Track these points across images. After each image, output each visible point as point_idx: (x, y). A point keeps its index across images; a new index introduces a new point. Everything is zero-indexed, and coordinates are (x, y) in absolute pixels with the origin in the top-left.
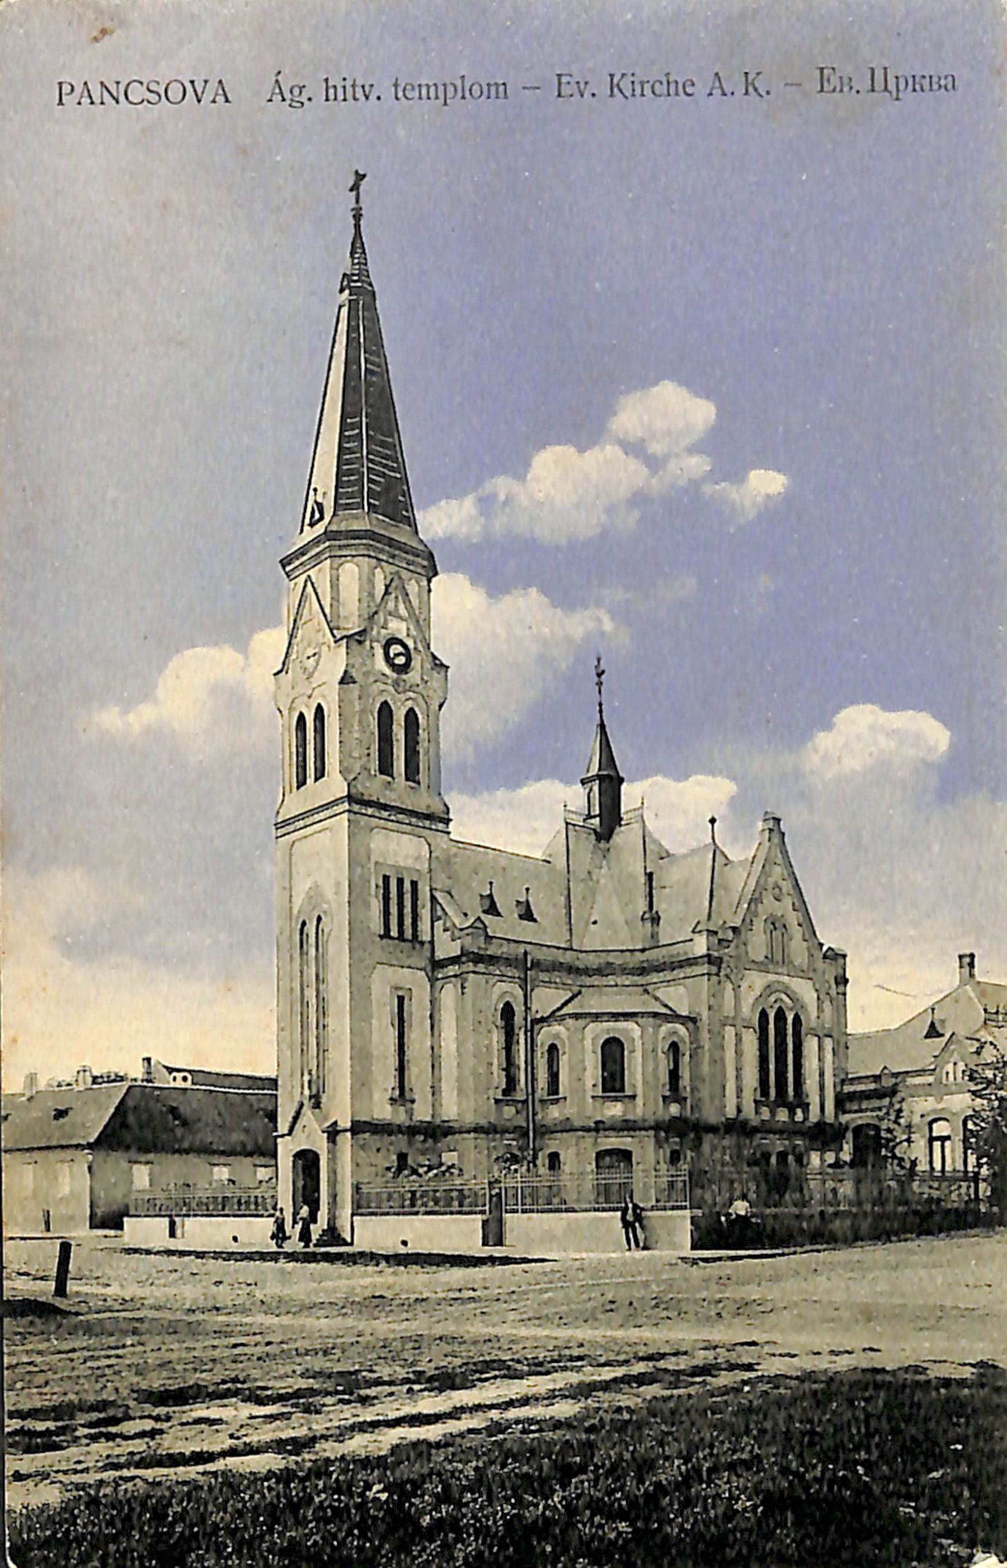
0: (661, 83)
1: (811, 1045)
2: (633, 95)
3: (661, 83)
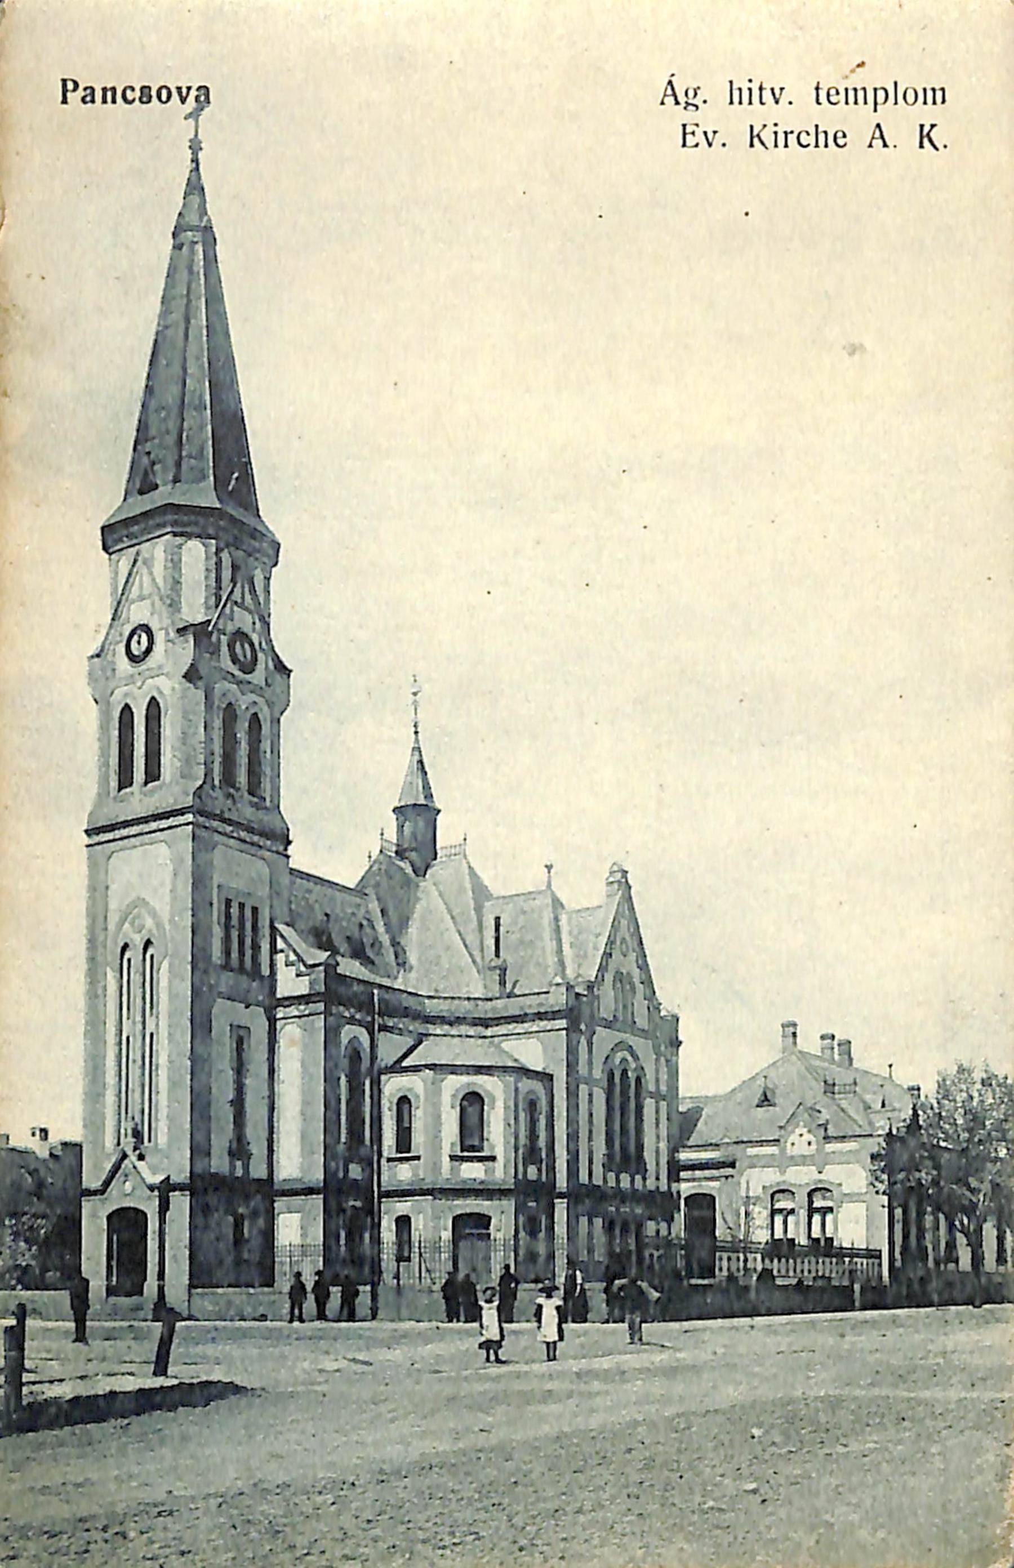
0: (808, 134)
1: (649, 1104)
2: (776, 146)
3: (808, 134)
